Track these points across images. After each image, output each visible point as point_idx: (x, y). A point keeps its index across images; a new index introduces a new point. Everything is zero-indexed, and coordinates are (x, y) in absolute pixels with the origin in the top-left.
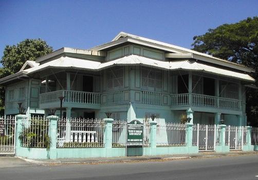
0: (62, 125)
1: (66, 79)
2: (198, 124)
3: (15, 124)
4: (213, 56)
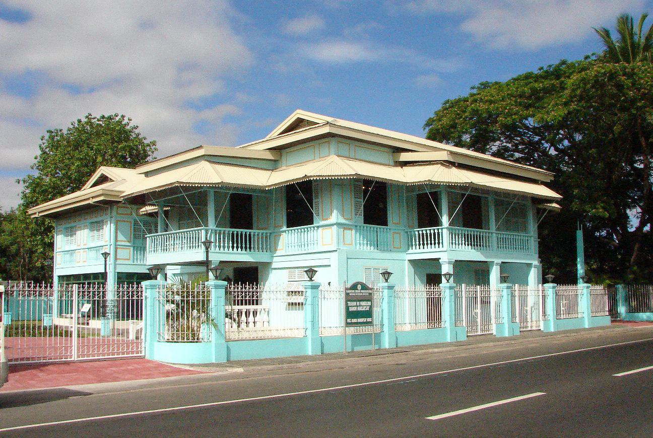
0: (247, 298)
1: (206, 205)
2: (463, 285)
3: (144, 298)
4: (494, 155)
